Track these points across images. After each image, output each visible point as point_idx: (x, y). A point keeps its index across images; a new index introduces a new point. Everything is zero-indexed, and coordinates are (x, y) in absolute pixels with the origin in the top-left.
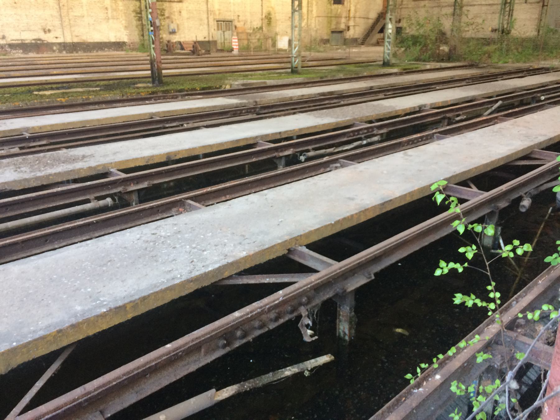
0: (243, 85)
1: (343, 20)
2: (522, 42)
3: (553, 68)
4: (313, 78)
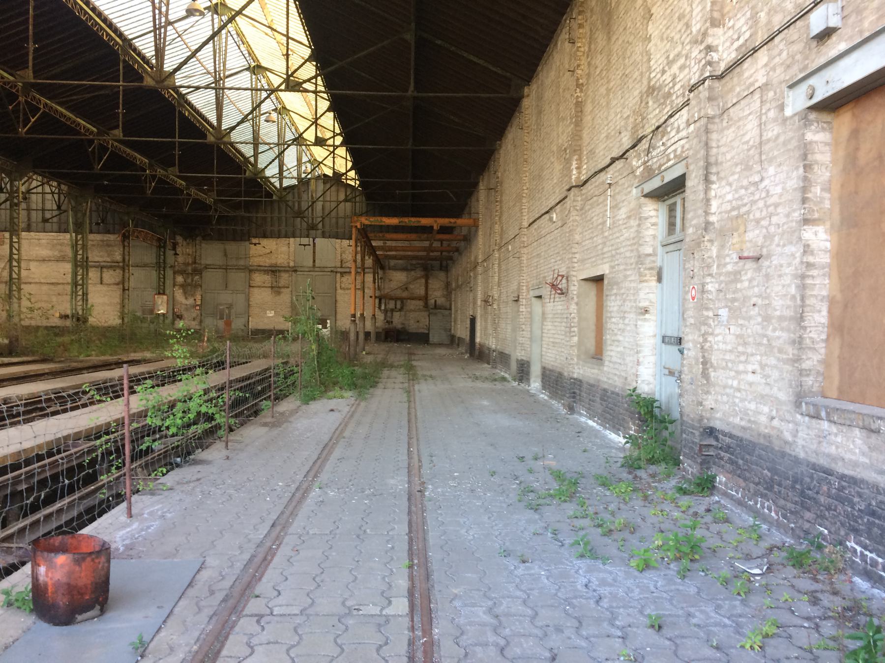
2: (105, 333)
3: (145, 360)
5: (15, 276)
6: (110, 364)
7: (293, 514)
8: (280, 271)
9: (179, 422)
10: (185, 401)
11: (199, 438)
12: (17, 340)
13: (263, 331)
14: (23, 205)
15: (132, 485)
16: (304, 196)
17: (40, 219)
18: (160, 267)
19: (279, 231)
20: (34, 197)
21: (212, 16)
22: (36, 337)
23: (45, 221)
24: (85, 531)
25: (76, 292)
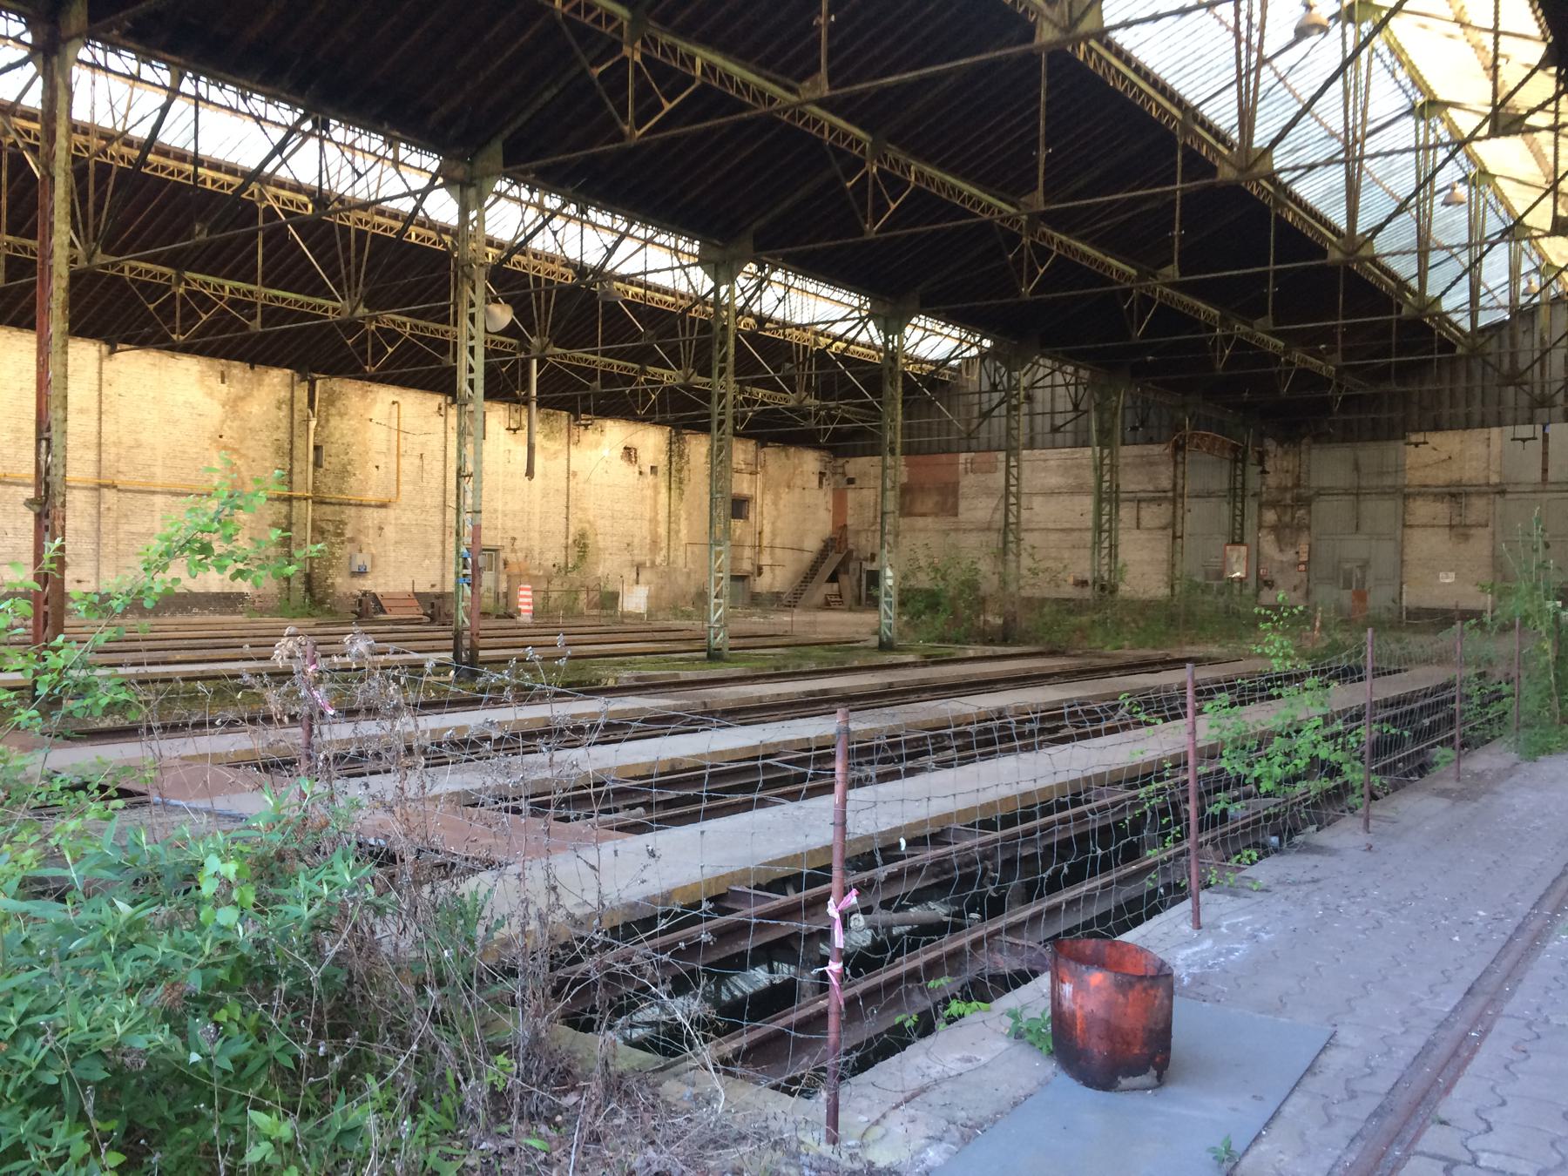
0: (638, 679)
1: (747, 553)
2: (1145, 608)
3: (1209, 659)
4: (762, 669)
5: (1012, 519)
6: (1154, 664)
7: (1513, 976)
8: (1467, 494)
9: (1277, 771)
10: (1289, 736)
11: (1315, 805)
12: (1014, 620)
13: (1431, 613)
14: (1025, 408)
15: (1199, 873)
16: (1524, 342)
17: (1048, 428)
18: (1235, 496)
19: (1468, 416)
20: (1039, 394)
21: (1343, 27)
22: (1042, 616)
23: (1055, 430)
24: (1128, 937)
25: (1100, 542)
